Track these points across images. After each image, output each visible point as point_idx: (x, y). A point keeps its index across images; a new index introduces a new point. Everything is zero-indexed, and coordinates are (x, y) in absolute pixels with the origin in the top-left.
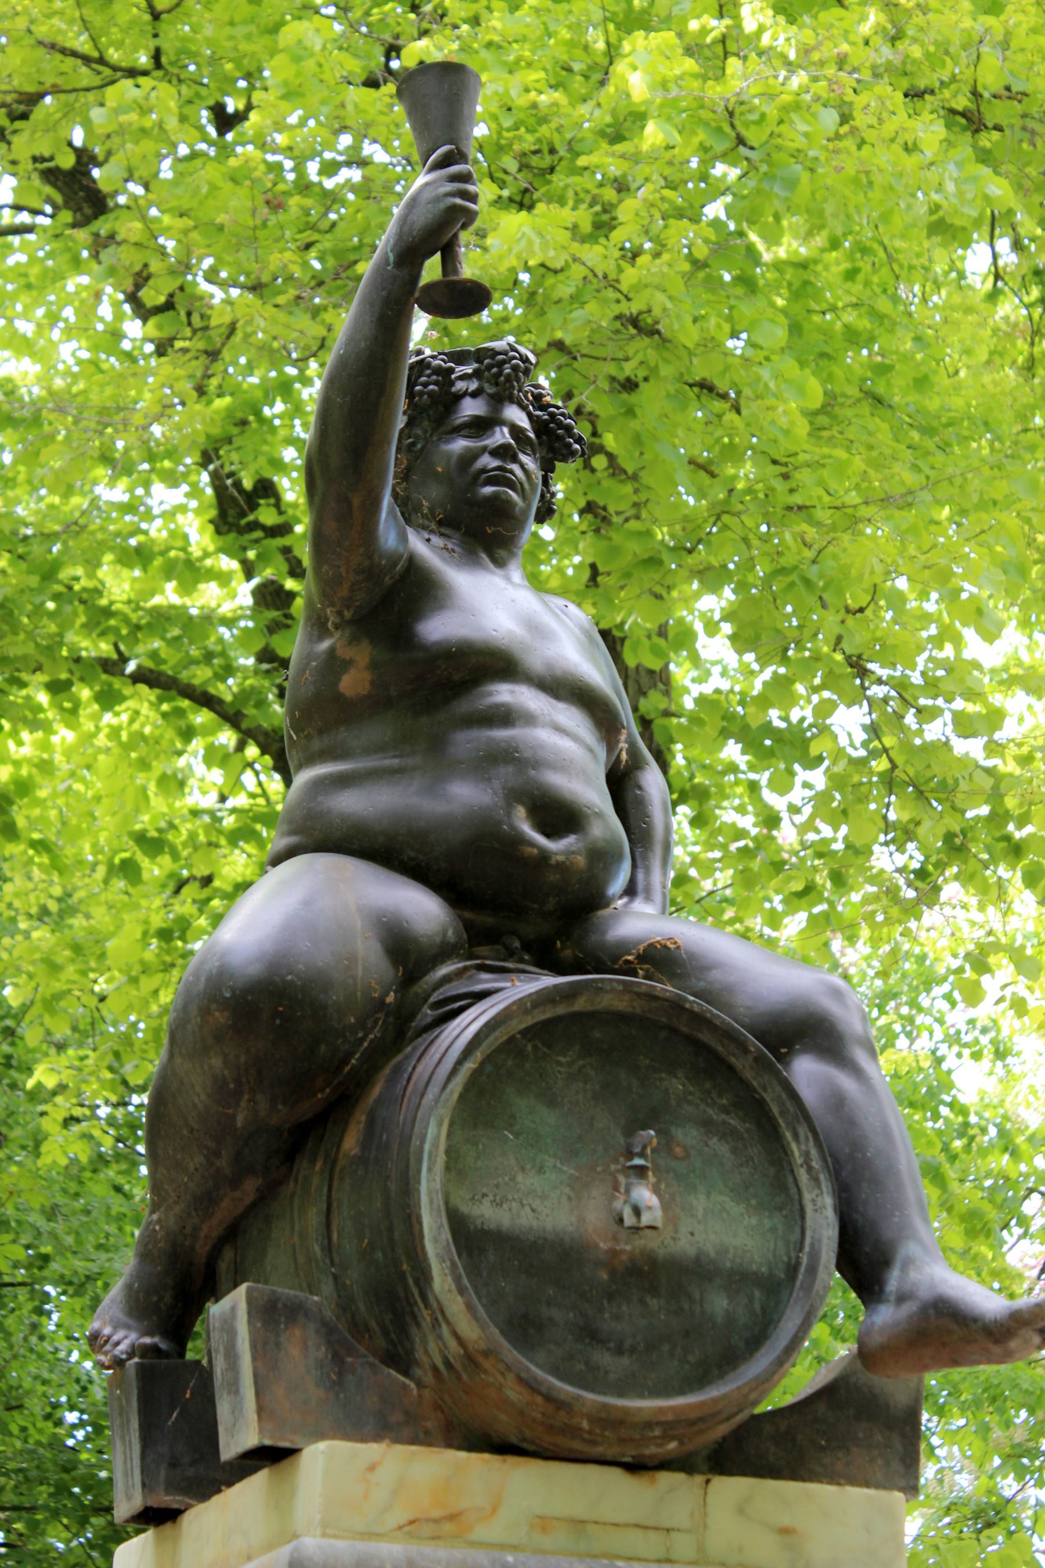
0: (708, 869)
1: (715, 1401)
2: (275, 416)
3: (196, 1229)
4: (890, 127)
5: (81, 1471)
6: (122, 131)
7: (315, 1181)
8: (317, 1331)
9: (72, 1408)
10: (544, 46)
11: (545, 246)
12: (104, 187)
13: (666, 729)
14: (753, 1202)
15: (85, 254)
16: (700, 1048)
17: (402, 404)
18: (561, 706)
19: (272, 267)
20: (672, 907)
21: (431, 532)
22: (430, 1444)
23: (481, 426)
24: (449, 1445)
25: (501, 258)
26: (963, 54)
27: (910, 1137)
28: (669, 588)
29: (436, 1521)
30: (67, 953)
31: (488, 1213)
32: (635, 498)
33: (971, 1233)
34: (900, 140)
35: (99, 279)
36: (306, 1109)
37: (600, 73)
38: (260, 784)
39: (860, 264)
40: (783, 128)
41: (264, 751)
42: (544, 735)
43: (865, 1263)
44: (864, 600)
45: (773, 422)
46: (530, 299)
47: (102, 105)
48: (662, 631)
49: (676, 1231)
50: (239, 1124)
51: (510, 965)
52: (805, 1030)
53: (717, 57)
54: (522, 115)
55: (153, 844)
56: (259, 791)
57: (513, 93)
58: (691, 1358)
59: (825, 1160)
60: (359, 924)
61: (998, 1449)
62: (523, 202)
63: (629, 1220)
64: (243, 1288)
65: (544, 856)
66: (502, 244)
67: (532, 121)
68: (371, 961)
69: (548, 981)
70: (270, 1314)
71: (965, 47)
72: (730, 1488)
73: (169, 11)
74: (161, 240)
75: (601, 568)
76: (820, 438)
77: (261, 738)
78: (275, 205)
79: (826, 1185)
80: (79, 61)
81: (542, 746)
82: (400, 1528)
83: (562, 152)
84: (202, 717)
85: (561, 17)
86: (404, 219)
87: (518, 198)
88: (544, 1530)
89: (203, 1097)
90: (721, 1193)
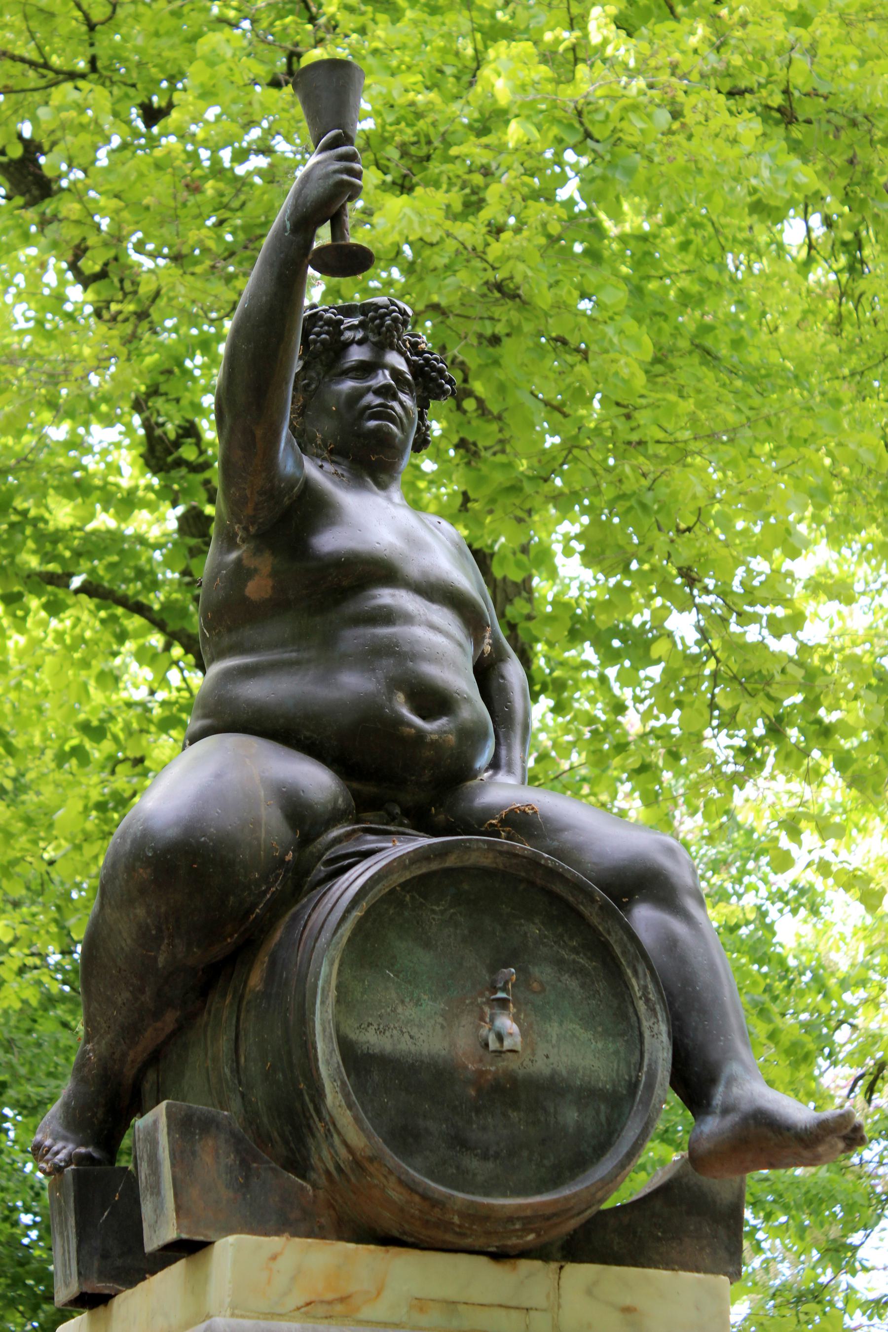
0: (565, 750)
1: (567, 1199)
2: (196, 367)
3: (124, 1055)
4: (715, 124)
5: (34, 1265)
6: (63, 126)
7: (226, 1013)
8: (227, 1141)
9: (27, 1210)
10: (421, 53)
11: (422, 223)
12: (48, 173)
13: (528, 630)
14: (600, 1029)
15: (33, 229)
16: (554, 898)
17: (298, 350)
18: (435, 607)
19: (191, 242)
20: (531, 780)
21: (324, 459)
22: (324, 1238)
23: (366, 369)
24: (340, 1238)
25: (385, 234)
26: (777, 59)
27: (735, 980)
28: (529, 512)
29: (330, 1303)
30: (21, 825)
31: (372, 1039)
32: (500, 436)
33: (795, 1065)
34: (723, 135)
35: (43, 251)
36: (218, 951)
37: (470, 74)
38: (184, 679)
39: (692, 236)
40: (624, 125)
41: (187, 652)
42: (420, 632)
43: (695, 1080)
44: (691, 520)
45: (616, 374)
46: (410, 269)
47: (46, 103)
48: (525, 549)
49: (534, 1054)
50: (160, 965)
51: (392, 828)
52: (643, 882)
53: (568, 62)
54: (402, 112)
55: (95, 731)
56: (184, 685)
57: (395, 94)
58: (546, 1162)
59: (660, 993)
60: (262, 793)
61: (815, 1244)
62: (404, 186)
63: (493, 1045)
64: (164, 1104)
65: (421, 735)
66: (383, 218)
67: (411, 117)
68: (272, 823)
69: (424, 841)
70: (186, 1127)
71: (778, 54)
72: (580, 1274)
73: (103, 23)
74: (97, 218)
75: (471, 495)
76: (655, 383)
77: (185, 640)
78: (194, 188)
79: (661, 1015)
80: (26, 66)
81: (418, 641)
82: (298, 1309)
83: (437, 143)
84: (135, 622)
85: (437, 28)
86: (299, 193)
87: (399, 181)
88: (421, 1310)
89: (129, 941)
90: (571, 1021)
